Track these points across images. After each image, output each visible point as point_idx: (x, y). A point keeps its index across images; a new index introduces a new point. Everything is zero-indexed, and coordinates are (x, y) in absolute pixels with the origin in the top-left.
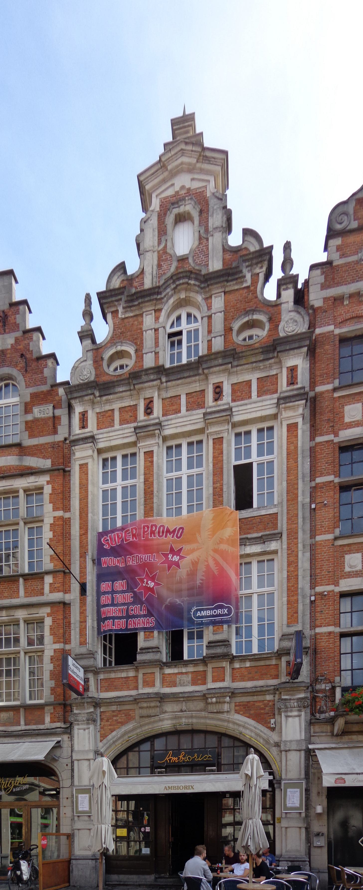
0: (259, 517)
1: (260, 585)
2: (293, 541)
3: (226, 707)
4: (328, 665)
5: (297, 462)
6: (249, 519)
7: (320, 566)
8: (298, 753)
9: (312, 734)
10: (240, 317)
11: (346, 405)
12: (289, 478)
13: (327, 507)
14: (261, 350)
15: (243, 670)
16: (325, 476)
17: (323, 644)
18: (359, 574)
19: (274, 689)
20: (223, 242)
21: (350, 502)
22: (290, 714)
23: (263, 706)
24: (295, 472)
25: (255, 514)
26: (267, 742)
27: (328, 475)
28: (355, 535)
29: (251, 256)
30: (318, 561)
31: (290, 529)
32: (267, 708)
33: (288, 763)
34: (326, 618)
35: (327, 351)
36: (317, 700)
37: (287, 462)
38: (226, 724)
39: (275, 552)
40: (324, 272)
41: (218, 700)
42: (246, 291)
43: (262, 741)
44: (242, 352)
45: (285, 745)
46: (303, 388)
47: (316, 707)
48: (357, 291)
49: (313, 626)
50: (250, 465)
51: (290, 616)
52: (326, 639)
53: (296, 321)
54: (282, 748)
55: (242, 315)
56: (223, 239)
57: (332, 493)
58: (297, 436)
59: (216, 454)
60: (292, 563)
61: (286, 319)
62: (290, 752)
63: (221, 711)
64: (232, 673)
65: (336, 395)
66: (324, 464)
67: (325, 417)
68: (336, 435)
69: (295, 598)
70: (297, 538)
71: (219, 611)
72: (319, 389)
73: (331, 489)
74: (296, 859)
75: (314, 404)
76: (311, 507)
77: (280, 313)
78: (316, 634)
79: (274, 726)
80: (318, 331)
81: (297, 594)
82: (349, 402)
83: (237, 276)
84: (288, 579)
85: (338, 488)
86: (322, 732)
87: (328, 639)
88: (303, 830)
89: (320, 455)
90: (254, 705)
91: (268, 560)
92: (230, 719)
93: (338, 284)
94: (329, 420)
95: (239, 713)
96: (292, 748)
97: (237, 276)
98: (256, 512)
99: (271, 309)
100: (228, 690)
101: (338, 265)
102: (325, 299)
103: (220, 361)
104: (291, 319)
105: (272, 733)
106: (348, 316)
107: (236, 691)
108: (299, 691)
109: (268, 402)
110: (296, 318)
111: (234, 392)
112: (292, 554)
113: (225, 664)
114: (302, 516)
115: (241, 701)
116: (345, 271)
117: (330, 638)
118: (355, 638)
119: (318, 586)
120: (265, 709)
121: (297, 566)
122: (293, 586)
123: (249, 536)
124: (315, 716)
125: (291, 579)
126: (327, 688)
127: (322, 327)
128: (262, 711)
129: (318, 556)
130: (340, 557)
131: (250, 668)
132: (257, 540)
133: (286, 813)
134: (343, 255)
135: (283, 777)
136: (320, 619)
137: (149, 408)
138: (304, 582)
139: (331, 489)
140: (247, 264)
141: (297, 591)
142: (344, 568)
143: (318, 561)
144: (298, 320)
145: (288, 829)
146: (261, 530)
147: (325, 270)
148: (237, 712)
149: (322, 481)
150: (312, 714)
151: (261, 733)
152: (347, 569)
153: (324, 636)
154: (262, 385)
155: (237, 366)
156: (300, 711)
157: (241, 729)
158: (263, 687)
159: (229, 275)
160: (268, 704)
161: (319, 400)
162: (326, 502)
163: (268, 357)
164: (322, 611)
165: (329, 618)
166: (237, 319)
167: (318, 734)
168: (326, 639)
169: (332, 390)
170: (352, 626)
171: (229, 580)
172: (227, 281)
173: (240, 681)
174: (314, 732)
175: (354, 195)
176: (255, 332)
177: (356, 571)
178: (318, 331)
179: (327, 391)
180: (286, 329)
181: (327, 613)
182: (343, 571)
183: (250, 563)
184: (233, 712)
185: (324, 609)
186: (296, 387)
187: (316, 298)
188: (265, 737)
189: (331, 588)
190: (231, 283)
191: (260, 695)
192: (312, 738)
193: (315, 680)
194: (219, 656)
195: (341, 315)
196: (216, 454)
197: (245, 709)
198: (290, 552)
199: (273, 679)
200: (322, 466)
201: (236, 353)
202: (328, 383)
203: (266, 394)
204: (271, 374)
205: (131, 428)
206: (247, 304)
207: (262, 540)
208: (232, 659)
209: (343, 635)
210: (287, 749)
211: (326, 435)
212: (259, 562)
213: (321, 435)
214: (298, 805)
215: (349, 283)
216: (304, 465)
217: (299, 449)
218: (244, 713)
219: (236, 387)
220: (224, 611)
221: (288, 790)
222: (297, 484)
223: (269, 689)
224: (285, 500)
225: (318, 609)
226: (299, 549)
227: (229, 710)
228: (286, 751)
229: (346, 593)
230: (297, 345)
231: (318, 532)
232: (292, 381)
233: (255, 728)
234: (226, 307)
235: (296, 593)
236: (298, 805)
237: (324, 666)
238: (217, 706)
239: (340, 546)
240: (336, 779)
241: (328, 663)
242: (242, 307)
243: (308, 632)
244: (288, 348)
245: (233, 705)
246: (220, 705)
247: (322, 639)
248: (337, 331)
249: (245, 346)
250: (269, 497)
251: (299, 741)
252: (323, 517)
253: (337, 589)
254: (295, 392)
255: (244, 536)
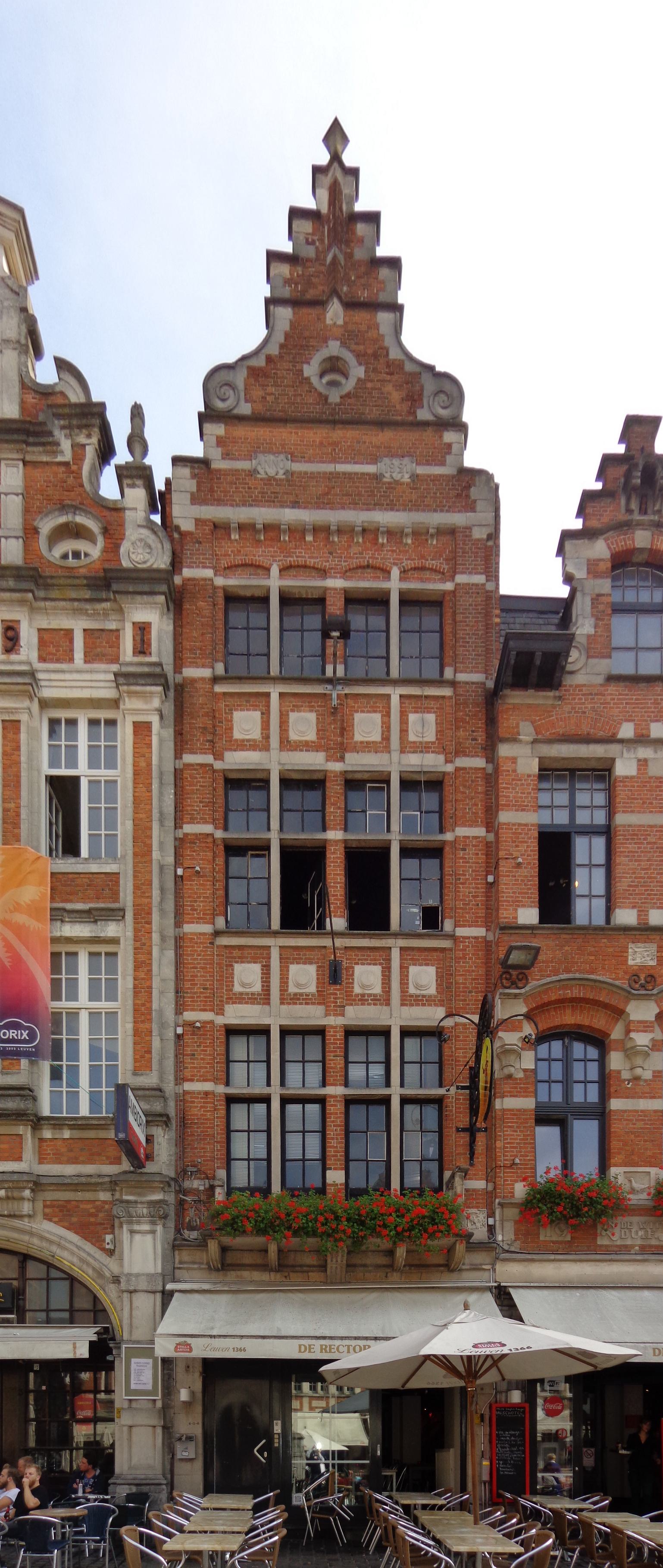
0: (87, 876)
1: (94, 995)
2: (143, 927)
3: (26, 1208)
4: (203, 1148)
5: (150, 791)
6: (71, 876)
7: (192, 976)
8: (151, 1296)
9: (177, 1265)
10: (50, 512)
11: (236, 710)
12: (137, 815)
13: (202, 877)
14: (85, 582)
15: (60, 1143)
16: (198, 823)
17: (195, 1110)
18: (256, 999)
19: (111, 1182)
20: (20, 370)
21: (244, 875)
22: (136, 1227)
23: (93, 1210)
24: (148, 807)
25: (81, 868)
26: (100, 1275)
27: (204, 823)
28: (251, 933)
29: (67, 411)
30: (187, 968)
31: (138, 905)
32: (101, 1215)
33: (134, 1312)
34: (201, 1068)
35: (201, 609)
36: (186, 1207)
37: (135, 787)
38: (26, 1238)
39: (115, 941)
40: (195, 475)
41: (10, 1194)
42: (63, 469)
43: (90, 1272)
44: (52, 577)
45: (128, 1281)
46: (160, 664)
47: (183, 1217)
48: (251, 521)
49: (180, 1080)
50: (75, 780)
51: (138, 1057)
52: (200, 1102)
53: (150, 547)
54: (123, 1286)
55: (55, 510)
56: (19, 364)
57: (210, 855)
58: (149, 745)
59: (8, 749)
60: (143, 965)
61: (133, 538)
62: (137, 1294)
63: (16, 1213)
64: (40, 1147)
65: (219, 689)
66: (196, 802)
67: (200, 722)
68: (219, 756)
69: (147, 1025)
70: (149, 923)
71: (12, 1034)
72: (190, 672)
73: (208, 847)
74: (144, 1482)
75: (180, 695)
76: (176, 872)
77: (122, 525)
78: (185, 1093)
79: (110, 1247)
80: (187, 572)
81: (150, 1020)
82: (240, 706)
83: (43, 440)
84: (135, 992)
85: (222, 847)
86: (194, 1263)
87: (204, 1103)
88: (159, 1431)
89: (190, 786)
90: (77, 1207)
91: (107, 954)
92: (34, 1230)
93: (219, 502)
94: (205, 728)
95: (50, 1220)
96: (140, 1288)
97: (43, 440)
98: (82, 866)
99: (106, 513)
100: (25, 1178)
101: (219, 470)
102: (199, 522)
103: (11, 583)
104: (141, 540)
105: (109, 1259)
106: (238, 560)
107: (44, 1181)
108: (153, 1189)
109: (102, 677)
110: (150, 542)
111: (42, 643)
112: (142, 949)
113: (24, 1130)
114: (158, 886)
115: (55, 1198)
116: (231, 483)
117: (207, 1103)
118: (309, 1107)
119: (187, 1010)
120: (96, 1216)
121: (151, 970)
122: (143, 1005)
123: (69, 906)
124: (181, 1235)
125: (141, 992)
126: (202, 1188)
127: (192, 567)
128: (92, 1220)
129: (187, 960)
130: (227, 966)
131: (71, 1141)
132: (84, 916)
133: (130, 1400)
134: (228, 454)
135: (125, 1338)
136: (192, 1068)
137: (10, 639)
138: (163, 1001)
139: (208, 847)
140: (62, 422)
141: (150, 1014)
142: (233, 986)
143: (187, 968)
144: (153, 546)
145: (134, 1429)
146: (91, 900)
147: (196, 471)
148: (47, 1217)
149: (194, 832)
150: (178, 1231)
151: (89, 1258)
152: (237, 988)
153: (197, 1098)
154: (93, 643)
155: (45, 599)
156: (153, 1223)
157: (54, 1248)
158: (91, 1176)
159: (28, 433)
160: (103, 1207)
161: (189, 692)
162: (198, 868)
163: (99, 597)
164: (194, 1055)
165: (206, 1068)
166: (46, 515)
167: (185, 1266)
168: (200, 1102)
169: (210, 679)
170: (304, 1085)
171: (32, 981)
172: (28, 444)
173: (54, 1163)
174: (181, 1262)
175: (244, 358)
176: (81, 545)
177: (252, 994)
178: (187, 572)
179: (203, 679)
180: (133, 556)
181: (202, 1059)
182: (231, 990)
183: (76, 954)
184: (40, 1216)
185: (196, 1051)
186: (147, 659)
187: (185, 514)
188: (96, 1265)
189: (207, 1016)
190: (35, 449)
191: (88, 1191)
192: (177, 1271)
193: (183, 1173)
194: (9, 1115)
195: (226, 555)
196: (8, 749)
197: (61, 1213)
198: (138, 944)
199: (111, 1163)
200: (193, 806)
201: (40, 577)
202: (203, 666)
203: (101, 661)
204: (106, 628)
205: (109, 672)
206: (65, 493)
207: (91, 916)
208: (37, 1122)
209: (231, 1100)
210: (132, 1288)
211: (201, 753)
212: (91, 954)
213: (192, 752)
214: (149, 1387)
215: (237, 505)
216: (164, 799)
217: (154, 768)
218: (60, 1221)
219: (46, 636)
220: (22, 1034)
221: (133, 1360)
222: (151, 829)
223: (100, 1180)
224: (130, 853)
225: (188, 1050)
226: (154, 943)
227: (31, 1213)
228: (131, 1292)
229: (234, 1028)
230: (146, 588)
231: (187, 918)
232: (142, 647)
233: (77, 1246)
234: (27, 487)
235: (148, 1017)
236: (149, 1387)
237: (196, 1148)
238: (10, 1205)
239: (226, 946)
240: (177, 1344)
241: (204, 1144)
242: (57, 497)
243: (170, 1087)
244: (131, 590)
245: (40, 1205)
246: (16, 1203)
247: (193, 1102)
248: (220, 581)
249: (62, 567)
250: (108, 841)
251: (153, 1275)
252: (196, 893)
253: (220, 1020)
254: (146, 669)
255: (61, 905)
